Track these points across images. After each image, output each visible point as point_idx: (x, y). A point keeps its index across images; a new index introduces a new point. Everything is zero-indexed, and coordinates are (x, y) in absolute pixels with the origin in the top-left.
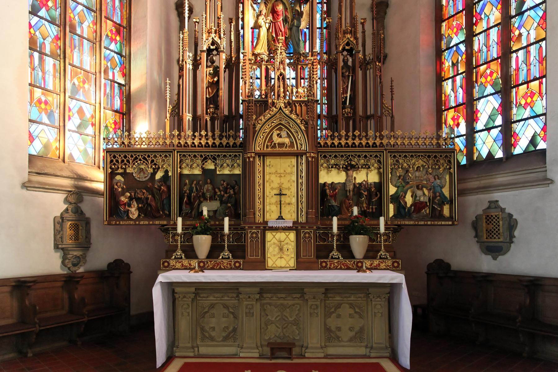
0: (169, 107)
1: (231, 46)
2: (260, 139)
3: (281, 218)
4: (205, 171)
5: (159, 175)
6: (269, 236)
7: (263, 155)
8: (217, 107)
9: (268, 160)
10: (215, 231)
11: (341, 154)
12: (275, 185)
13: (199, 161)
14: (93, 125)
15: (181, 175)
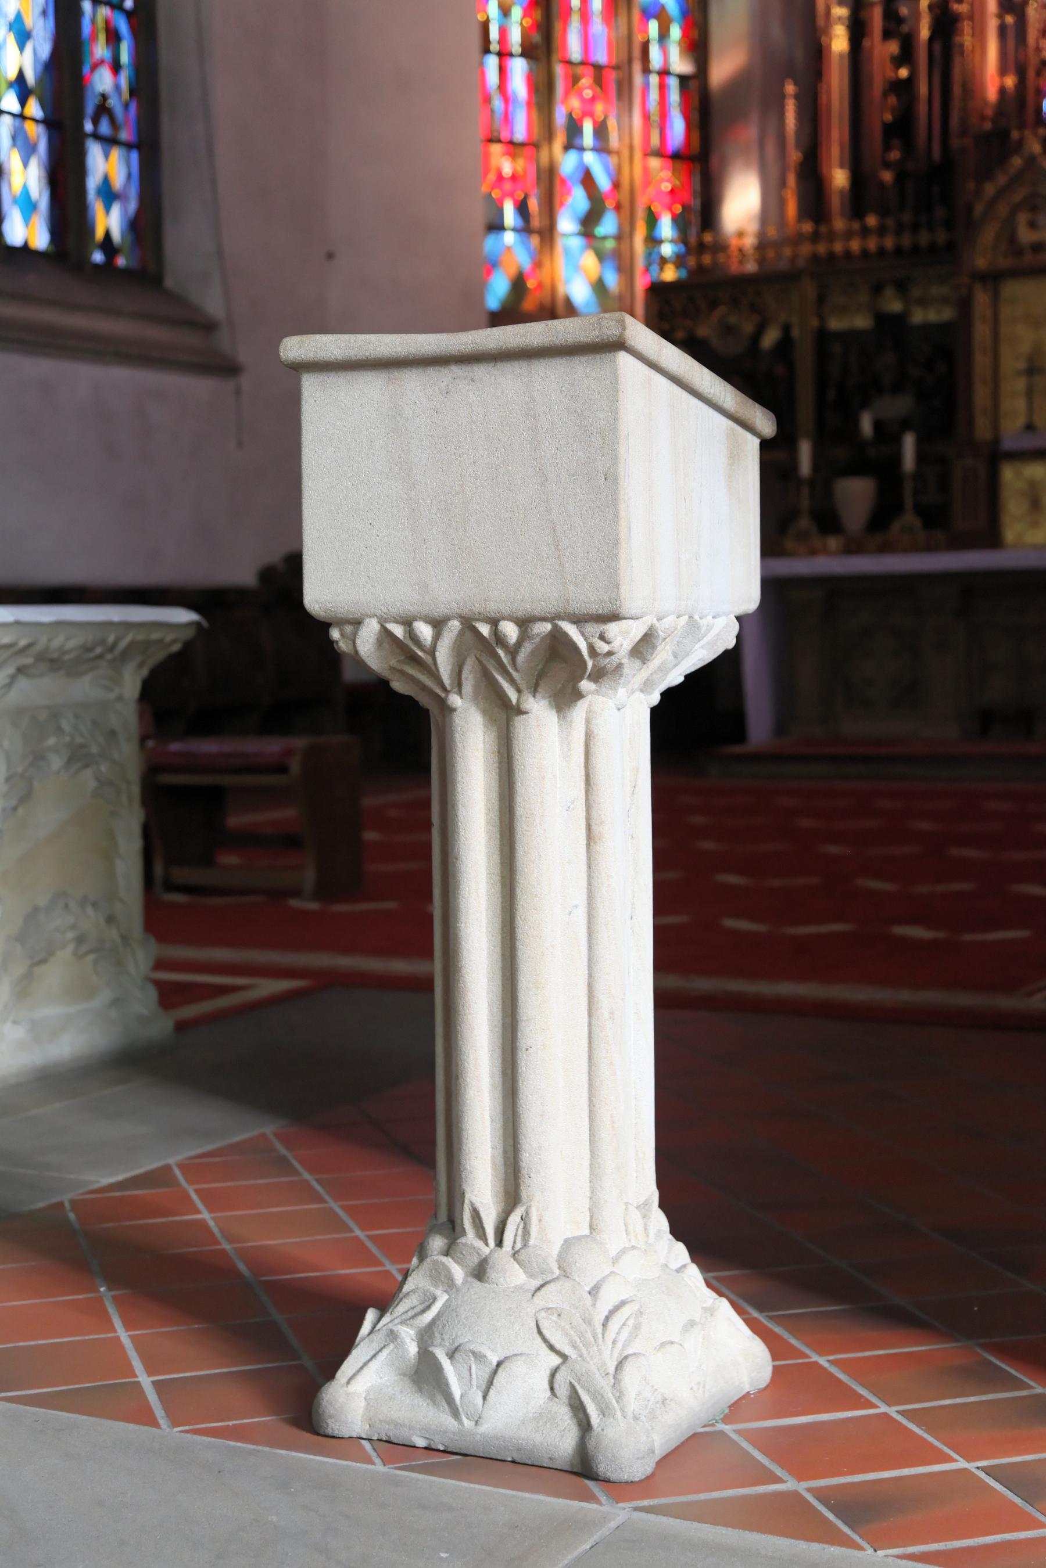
0: (795, 156)
1: (238, 770)
2: (988, 235)
3: (1030, 427)
4: (882, 319)
5: (770, 338)
6: (1008, 473)
7: (993, 279)
8: (908, 146)
9: (1012, 289)
10: (885, 471)
11: (559, 331)
12: (1025, 348)
13: (864, 297)
14: (618, 208)
15: (823, 336)
